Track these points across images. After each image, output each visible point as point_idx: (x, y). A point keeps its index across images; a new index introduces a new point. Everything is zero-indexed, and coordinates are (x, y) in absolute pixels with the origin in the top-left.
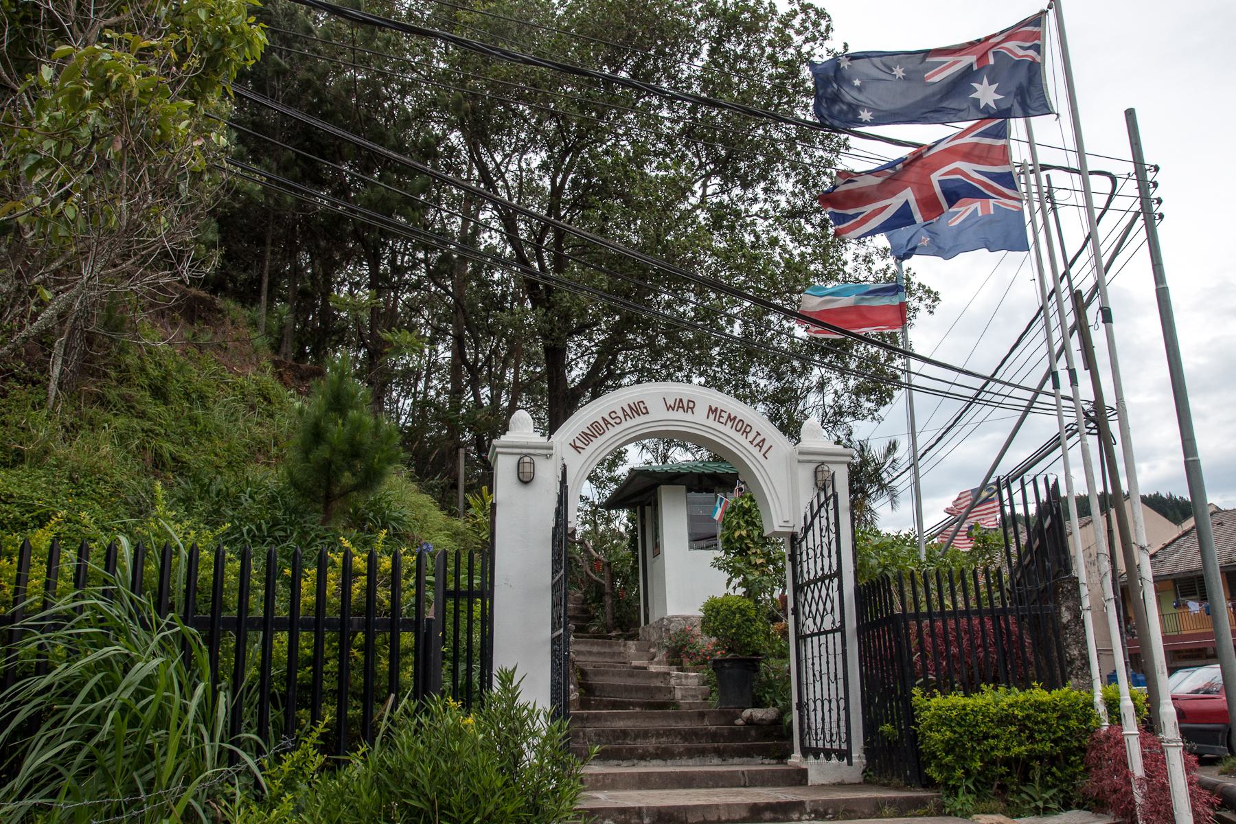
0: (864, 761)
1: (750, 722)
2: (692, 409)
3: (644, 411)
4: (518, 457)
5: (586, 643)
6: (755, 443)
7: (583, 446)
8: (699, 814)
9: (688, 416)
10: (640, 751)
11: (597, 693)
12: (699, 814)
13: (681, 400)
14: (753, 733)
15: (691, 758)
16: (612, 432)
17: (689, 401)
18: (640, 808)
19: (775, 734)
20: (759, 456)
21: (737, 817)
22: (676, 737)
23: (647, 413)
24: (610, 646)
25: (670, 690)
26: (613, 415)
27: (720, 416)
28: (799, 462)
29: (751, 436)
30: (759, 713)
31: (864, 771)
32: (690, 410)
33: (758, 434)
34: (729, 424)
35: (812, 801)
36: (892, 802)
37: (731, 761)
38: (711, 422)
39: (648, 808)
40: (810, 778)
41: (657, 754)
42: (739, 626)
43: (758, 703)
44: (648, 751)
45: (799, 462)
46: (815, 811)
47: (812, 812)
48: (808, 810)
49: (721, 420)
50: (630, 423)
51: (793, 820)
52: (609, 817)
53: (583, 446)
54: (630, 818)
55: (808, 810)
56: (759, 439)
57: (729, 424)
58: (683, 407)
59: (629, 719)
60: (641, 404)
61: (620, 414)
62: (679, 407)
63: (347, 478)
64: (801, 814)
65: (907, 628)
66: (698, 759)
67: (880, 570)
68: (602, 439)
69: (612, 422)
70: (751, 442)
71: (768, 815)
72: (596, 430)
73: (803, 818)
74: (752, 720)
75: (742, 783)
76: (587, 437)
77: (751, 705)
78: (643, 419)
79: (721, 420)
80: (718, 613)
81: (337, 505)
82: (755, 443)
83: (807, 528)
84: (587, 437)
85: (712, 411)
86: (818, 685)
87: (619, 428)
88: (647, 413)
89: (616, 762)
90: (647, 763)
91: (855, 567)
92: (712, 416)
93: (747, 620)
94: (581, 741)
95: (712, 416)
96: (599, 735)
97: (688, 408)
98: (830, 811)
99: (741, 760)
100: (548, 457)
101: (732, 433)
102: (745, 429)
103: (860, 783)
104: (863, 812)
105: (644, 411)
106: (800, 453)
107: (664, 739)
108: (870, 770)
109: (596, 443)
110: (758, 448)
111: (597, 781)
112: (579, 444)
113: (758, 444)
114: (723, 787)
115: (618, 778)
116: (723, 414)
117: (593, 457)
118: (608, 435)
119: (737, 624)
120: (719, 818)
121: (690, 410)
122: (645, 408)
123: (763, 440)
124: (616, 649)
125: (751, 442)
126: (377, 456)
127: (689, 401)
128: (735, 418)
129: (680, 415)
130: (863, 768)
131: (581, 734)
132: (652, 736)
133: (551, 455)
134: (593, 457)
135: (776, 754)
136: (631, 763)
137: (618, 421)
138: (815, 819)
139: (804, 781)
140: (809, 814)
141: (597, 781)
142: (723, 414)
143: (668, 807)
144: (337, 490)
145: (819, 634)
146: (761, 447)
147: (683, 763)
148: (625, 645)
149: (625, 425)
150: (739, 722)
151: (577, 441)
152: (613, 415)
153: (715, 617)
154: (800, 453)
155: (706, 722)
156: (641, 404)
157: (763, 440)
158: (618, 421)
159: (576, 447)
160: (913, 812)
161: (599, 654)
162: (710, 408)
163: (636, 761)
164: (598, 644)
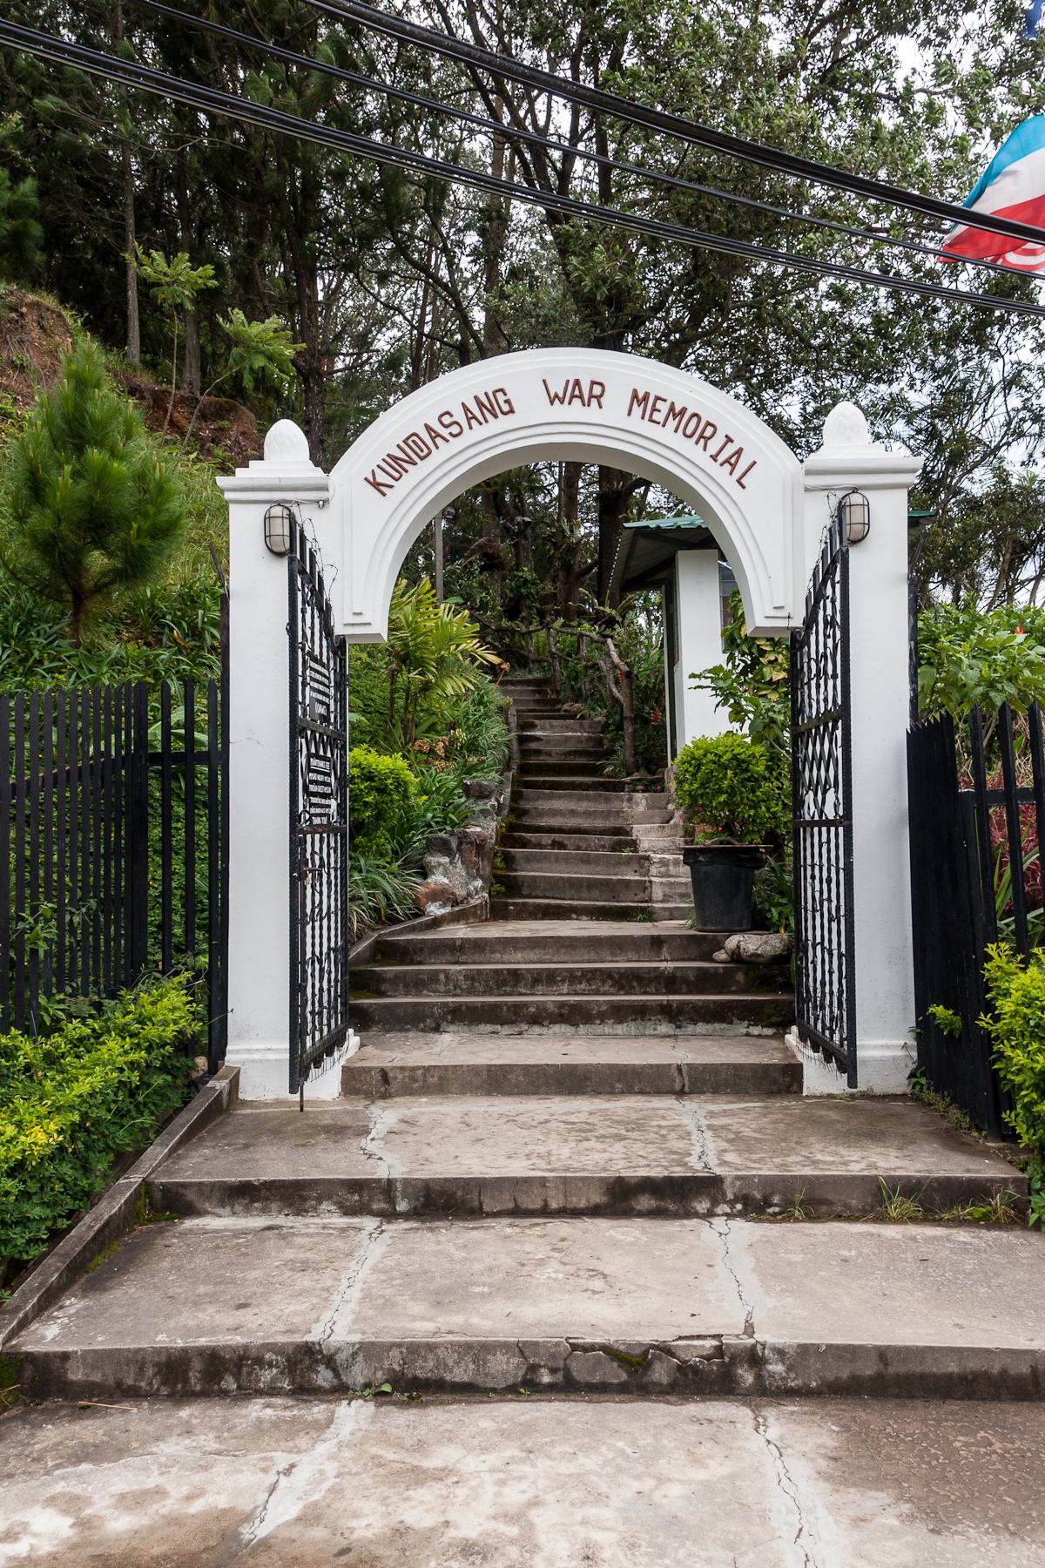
0: (914, 1054)
1: (736, 957)
2: (598, 398)
3: (506, 408)
4: (268, 506)
5: (570, 797)
6: (721, 458)
7: (390, 481)
8: (506, 1196)
9: (592, 413)
10: (532, 1010)
11: (525, 891)
12: (506, 1196)
13: (577, 383)
14: (740, 977)
15: (621, 1022)
16: (444, 451)
17: (593, 383)
18: (390, 1182)
19: (780, 979)
20: (730, 483)
21: (583, 1204)
22: (604, 982)
23: (512, 411)
24: (607, 800)
25: (645, 887)
26: (447, 420)
27: (654, 410)
28: (807, 490)
29: (714, 446)
30: (751, 943)
31: (912, 1075)
32: (594, 401)
33: (729, 440)
34: (672, 423)
35: (738, 1178)
36: (910, 1188)
37: (690, 1028)
38: (636, 423)
39: (406, 1182)
40: (806, 1083)
41: (561, 1015)
42: (732, 791)
43: (760, 923)
44: (545, 1009)
45: (807, 490)
46: (745, 1199)
47: (736, 1200)
48: (730, 1196)
49: (656, 416)
50: (479, 432)
51: (697, 1215)
52: (329, 1198)
53: (390, 481)
54: (371, 1200)
55: (730, 1196)
56: (730, 449)
57: (672, 423)
58: (581, 397)
59: (532, 948)
60: (500, 396)
61: (460, 416)
62: (573, 396)
63: (97, 561)
64: (715, 1203)
65: (985, 820)
66: (632, 1024)
67: (980, 690)
68: (424, 467)
69: (444, 432)
70: (714, 458)
71: (645, 1202)
72: (412, 451)
73: (719, 1210)
74: (739, 954)
75: (677, 1087)
76: (397, 464)
77: (746, 924)
78: (504, 423)
79: (656, 416)
80: (699, 766)
81: (94, 606)
82: (721, 458)
83: (810, 620)
84: (397, 464)
85: (638, 399)
86: (818, 915)
87: (456, 444)
88: (512, 411)
89: (489, 1028)
90: (544, 1030)
91: (914, 690)
92: (637, 410)
93: (748, 780)
94: (442, 988)
95: (637, 410)
96: (473, 979)
97: (591, 396)
98: (776, 1200)
99: (708, 1028)
100: (323, 504)
101: (678, 441)
102: (702, 432)
103: (903, 1097)
104: (846, 1206)
105: (506, 408)
106: (808, 473)
107: (583, 986)
108: (923, 1074)
109: (414, 474)
110: (727, 467)
111: (413, 1079)
112: (382, 478)
113: (727, 461)
114: (641, 1092)
115: (451, 1076)
116: (659, 405)
117: (410, 502)
118: (436, 457)
119: (731, 787)
120: (546, 1205)
121: (594, 401)
122: (507, 401)
123: (739, 452)
124: (615, 805)
125: (714, 458)
126: (135, 525)
127: (593, 383)
128: (684, 410)
129: (575, 411)
130: (912, 1067)
131: (442, 976)
132: (563, 981)
133: (326, 502)
134: (410, 502)
135: (774, 1019)
136: (516, 1029)
137: (455, 429)
138: (742, 1214)
139: (795, 1088)
140: (732, 1203)
141: (413, 1079)
142: (659, 405)
143: (446, 1180)
144: (89, 584)
145: (820, 824)
146: (733, 466)
147: (607, 1030)
148: (630, 799)
149: (469, 437)
150: (721, 955)
151: (378, 472)
152: (447, 420)
153: (694, 775)
154: (808, 473)
155: (665, 953)
156: (500, 396)
157: (739, 452)
158: (455, 429)
159: (376, 485)
160: (959, 1212)
161: (587, 814)
162: (635, 395)
163: (524, 1027)
164: (588, 798)
